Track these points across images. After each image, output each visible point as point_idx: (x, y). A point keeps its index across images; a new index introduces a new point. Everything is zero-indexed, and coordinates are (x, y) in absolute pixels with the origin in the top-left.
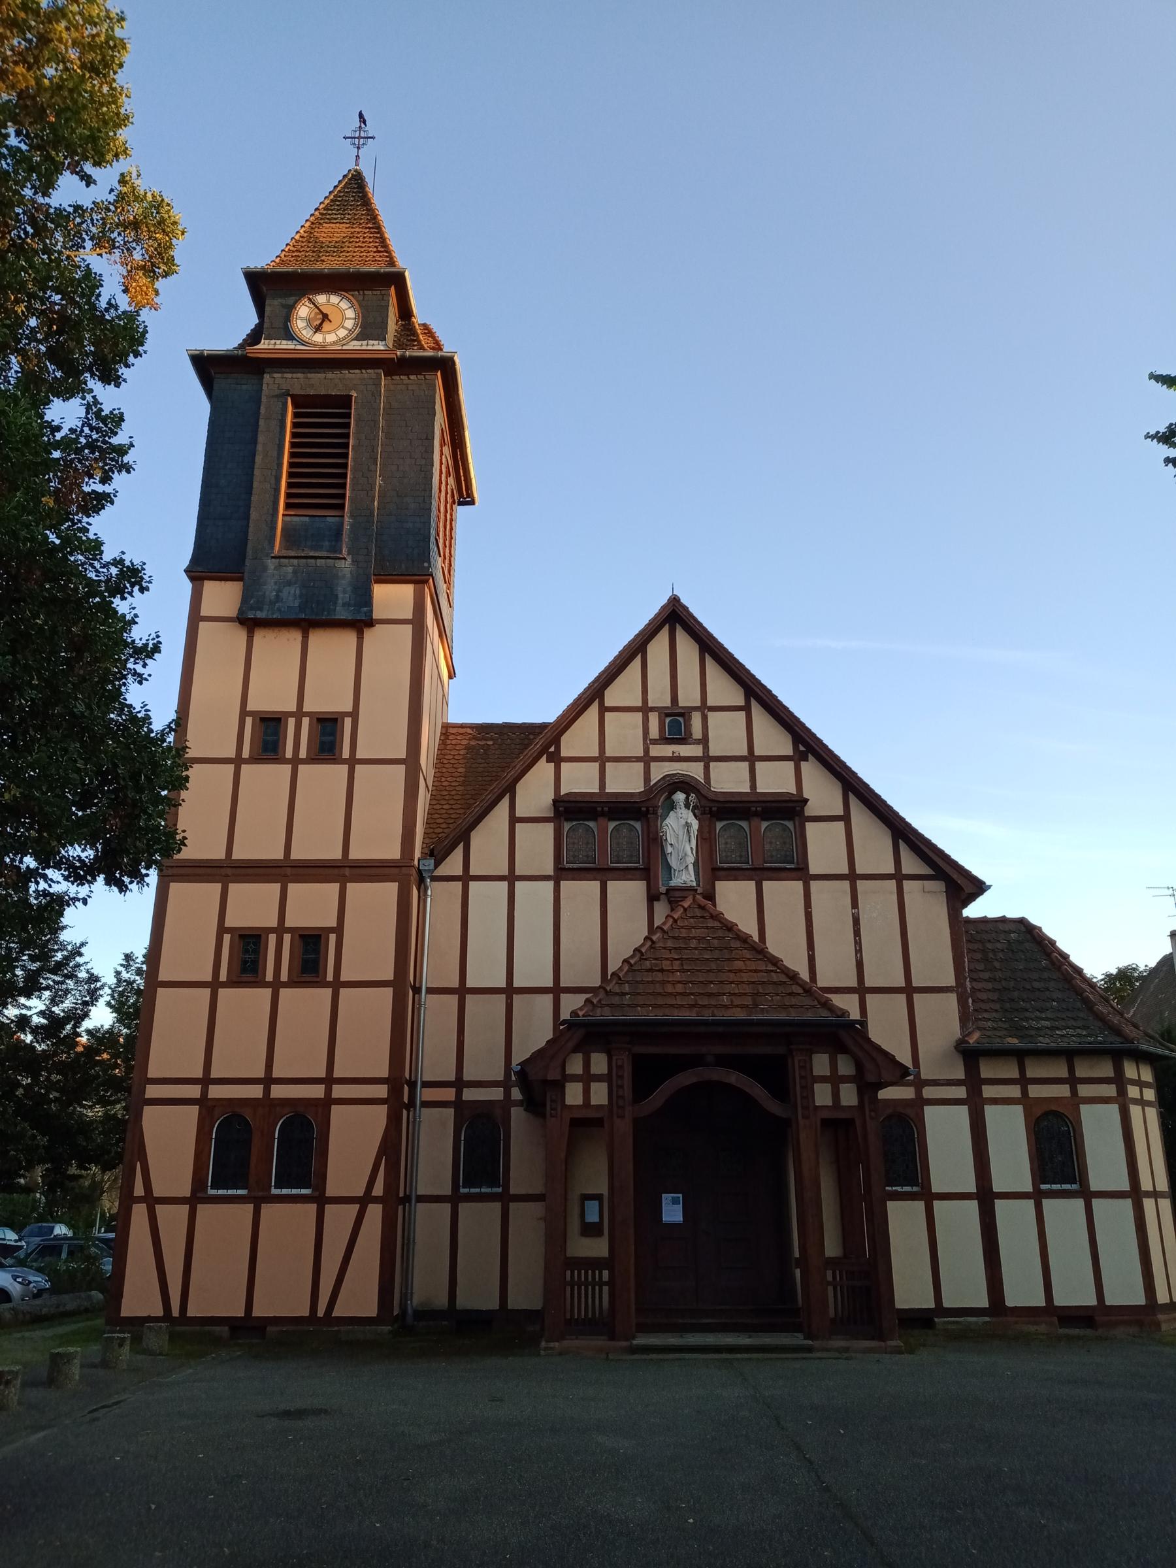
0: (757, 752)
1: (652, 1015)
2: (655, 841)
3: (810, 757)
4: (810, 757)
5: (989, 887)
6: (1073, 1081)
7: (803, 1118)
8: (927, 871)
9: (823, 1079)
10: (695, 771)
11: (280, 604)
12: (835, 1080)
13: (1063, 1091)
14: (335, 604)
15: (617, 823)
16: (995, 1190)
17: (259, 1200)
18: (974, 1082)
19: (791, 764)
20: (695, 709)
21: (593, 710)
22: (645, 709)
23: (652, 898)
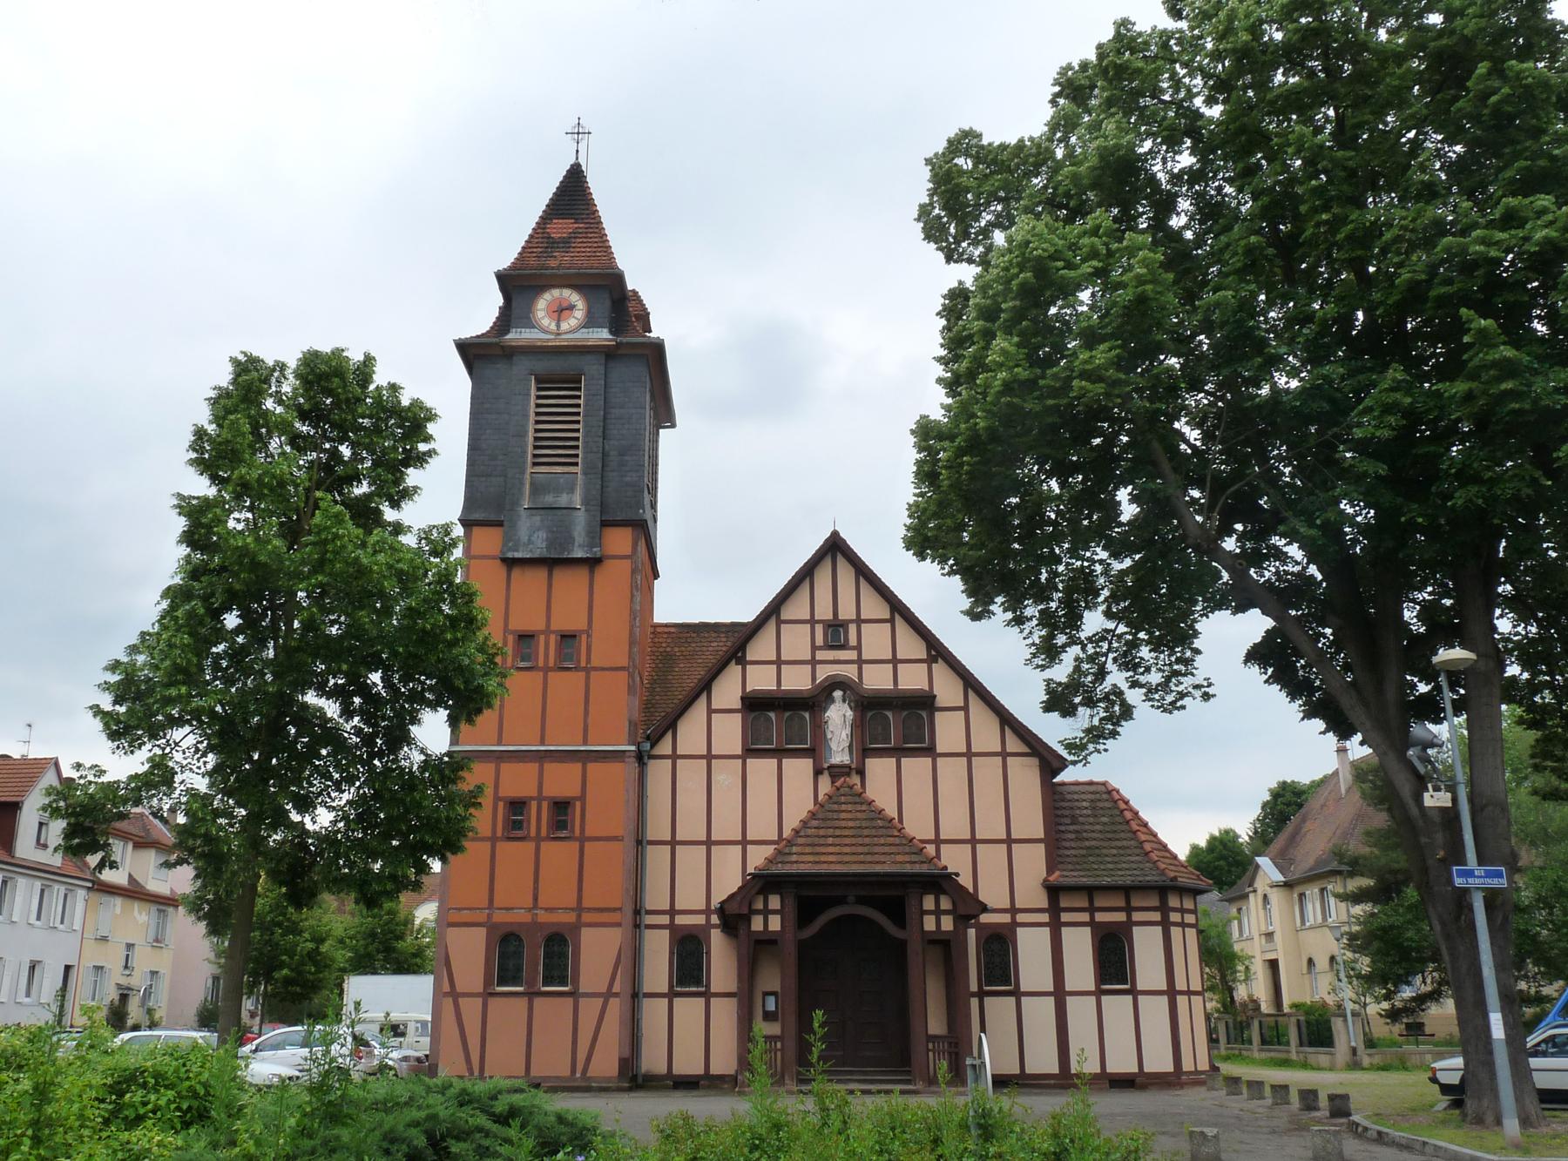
2: (819, 727)
6: (1129, 909)
8: (1026, 750)
10: (850, 672)
12: (938, 913)
13: (1120, 917)
17: (532, 995)
18: (1054, 909)
20: (852, 621)
22: (812, 622)
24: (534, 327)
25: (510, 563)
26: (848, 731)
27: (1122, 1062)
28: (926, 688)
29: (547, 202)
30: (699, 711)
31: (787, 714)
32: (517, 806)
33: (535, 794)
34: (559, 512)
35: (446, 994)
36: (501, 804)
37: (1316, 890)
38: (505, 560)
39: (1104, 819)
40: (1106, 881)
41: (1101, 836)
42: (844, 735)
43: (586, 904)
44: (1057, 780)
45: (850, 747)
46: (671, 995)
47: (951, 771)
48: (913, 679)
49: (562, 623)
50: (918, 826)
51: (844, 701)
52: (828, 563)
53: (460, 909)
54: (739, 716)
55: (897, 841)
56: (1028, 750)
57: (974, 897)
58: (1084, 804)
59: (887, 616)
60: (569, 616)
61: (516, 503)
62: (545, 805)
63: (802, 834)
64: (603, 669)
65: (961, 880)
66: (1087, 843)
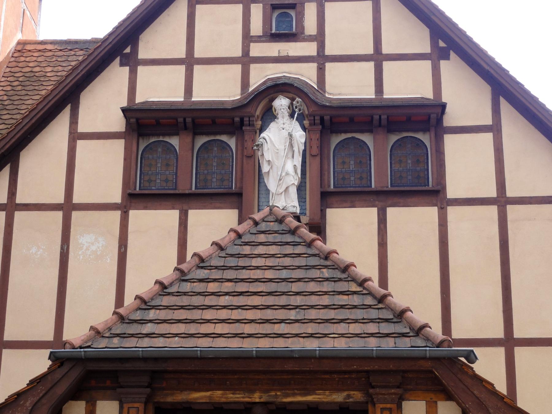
0: (386, 50)
3: (452, 55)
4: (452, 55)
19: (428, 64)
28: (429, 94)
31: (201, 140)
42: (289, 167)
45: (301, 189)
51: (292, 116)
54: (119, 145)
55: (356, 300)
63: (174, 289)
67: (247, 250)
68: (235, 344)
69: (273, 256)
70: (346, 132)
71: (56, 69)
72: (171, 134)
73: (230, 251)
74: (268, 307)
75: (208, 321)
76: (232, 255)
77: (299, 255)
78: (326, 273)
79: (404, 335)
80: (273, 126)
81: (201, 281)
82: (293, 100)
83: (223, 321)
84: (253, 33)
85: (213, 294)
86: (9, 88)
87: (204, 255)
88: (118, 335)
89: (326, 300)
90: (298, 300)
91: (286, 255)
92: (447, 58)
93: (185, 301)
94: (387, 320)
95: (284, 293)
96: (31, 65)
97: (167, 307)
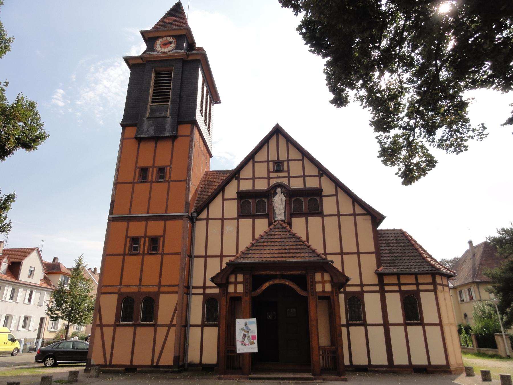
1: (257, 260)
2: (271, 205)
3: (324, 175)
5: (386, 217)
6: (417, 284)
7: (311, 296)
8: (365, 212)
9: (319, 282)
10: (285, 181)
11: (148, 132)
12: (323, 282)
13: (414, 288)
14: (165, 131)
15: (259, 199)
16: (389, 323)
17: (135, 326)
18: (381, 284)
19: (317, 178)
20: (285, 161)
21: (251, 163)
22: (268, 161)
23: (270, 224)
24: (155, 51)
25: (140, 140)
26: (284, 205)
27: (419, 360)
28: (318, 187)
29: (166, 12)
30: (219, 199)
31: (257, 200)
32: (135, 240)
33: (143, 235)
34: (160, 119)
35: (98, 325)
36: (128, 240)
37: (467, 290)
38: (136, 138)
39: (402, 244)
40: (406, 270)
41: (402, 251)
42: (281, 207)
43: (163, 283)
44: (379, 228)
45: (285, 213)
46: (203, 326)
47: (331, 223)
48: (312, 183)
49: (160, 163)
50: (317, 245)
51: (282, 193)
52: (274, 138)
53: (107, 286)
54: (236, 202)
55: (302, 247)
56: (366, 213)
57: (342, 274)
58: (392, 238)
59: (301, 158)
60: (162, 160)
61: (143, 116)
62: (147, 239)
63: (255, 245)
64: (176, 181)
65: (334, 265)
66: (395, 255)
67: (273, 233)
68: (272, 260)
69: (280, 235)
70: (296, 197)
71: (216, 179)
72: (250, 198)
73: (268, 234)
74: (280, 249)
75: (265, 253)
76: (270, 235)
77: (287, 234)
78: (294, 239)
79: (315, 256)
80: (277, 196)
81: (262, 242)
82: (282, 189)
83: (268, 253)
84: (270, 170)
85: (265, 246)
86: (204, 185)
87: (262, 235)
88: (242, 258)
89: (294, 247)
90: (287, 247)
91: (283, 235)
92: (323, 176)
93: (258, 248)
94: (311, 252)
95: (283, 245)
96: (209, 178)
97: (254, 250)
